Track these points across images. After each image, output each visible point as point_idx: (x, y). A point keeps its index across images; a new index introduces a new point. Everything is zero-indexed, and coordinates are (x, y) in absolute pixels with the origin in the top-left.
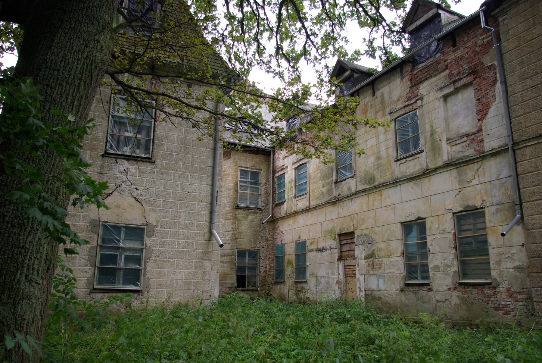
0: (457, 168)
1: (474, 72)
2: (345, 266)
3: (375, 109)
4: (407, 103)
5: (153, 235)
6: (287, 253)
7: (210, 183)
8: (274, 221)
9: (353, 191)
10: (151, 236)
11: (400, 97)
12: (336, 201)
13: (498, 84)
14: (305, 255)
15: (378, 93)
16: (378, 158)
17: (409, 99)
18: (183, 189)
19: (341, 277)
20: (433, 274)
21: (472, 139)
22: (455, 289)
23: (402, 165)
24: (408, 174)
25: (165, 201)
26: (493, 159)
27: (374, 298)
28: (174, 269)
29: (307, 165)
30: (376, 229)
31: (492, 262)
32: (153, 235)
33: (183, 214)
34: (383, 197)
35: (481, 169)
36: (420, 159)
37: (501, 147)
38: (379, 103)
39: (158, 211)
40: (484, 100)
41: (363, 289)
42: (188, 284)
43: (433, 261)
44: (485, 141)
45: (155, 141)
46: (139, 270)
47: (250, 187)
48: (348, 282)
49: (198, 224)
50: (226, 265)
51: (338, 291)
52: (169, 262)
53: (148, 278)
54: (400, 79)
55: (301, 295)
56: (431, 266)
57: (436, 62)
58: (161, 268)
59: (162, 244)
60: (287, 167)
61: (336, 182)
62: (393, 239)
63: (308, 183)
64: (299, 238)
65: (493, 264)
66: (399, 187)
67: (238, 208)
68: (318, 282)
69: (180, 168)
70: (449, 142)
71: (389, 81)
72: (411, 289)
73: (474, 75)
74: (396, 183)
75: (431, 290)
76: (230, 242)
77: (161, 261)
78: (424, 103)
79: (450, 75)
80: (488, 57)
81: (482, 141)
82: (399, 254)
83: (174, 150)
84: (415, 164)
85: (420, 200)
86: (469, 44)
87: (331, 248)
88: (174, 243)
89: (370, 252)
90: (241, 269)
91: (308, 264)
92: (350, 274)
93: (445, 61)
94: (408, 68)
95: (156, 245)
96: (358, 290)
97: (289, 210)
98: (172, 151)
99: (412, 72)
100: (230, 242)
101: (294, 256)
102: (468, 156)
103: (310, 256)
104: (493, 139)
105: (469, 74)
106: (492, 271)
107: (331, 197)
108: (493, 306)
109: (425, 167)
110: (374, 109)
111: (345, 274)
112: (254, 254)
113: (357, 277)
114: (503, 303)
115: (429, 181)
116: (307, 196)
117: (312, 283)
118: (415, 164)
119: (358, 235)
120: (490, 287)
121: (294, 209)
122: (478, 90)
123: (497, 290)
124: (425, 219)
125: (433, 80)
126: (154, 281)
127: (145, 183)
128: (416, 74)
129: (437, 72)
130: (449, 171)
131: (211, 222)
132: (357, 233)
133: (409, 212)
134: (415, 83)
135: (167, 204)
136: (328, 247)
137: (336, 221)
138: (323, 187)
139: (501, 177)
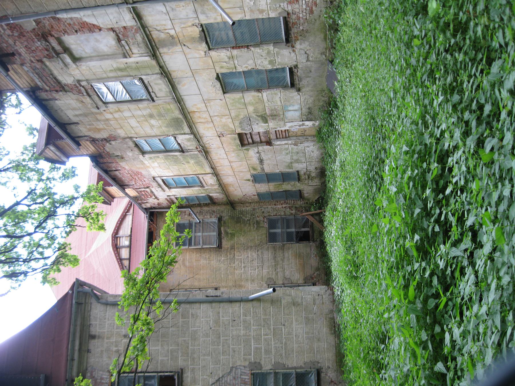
0: (158, 49)
1: (44, 36)
2: (277, 138)
3: (94, 121)
4: (85, 94)
5: (259, 363)
6: (268, 190)
7: (197, 305)
8: (231, 204)
9: (192, 136)
10: (261, 365)
11: (77, 100)
12: (206, 152)
13: (59, 16)
14: (267, 175)
15: (75, 119)
16: (151, 116)
17: (80, 92)
18: (207, 335)
19: (290, 142)
20: (278, 65)
21: (123, 35)
22: (293, 47)
23: (158, 95)
24: (167, 90)
25: (223, 353)
26: (144, 18)
27: (310, 113)
28: (293, 338)
29: (164, 178)
30: (233, 115)
31: (260, 17)
32: (259, 363)
33: (234, 333)
34: (196, 111)
35: (157, 28)
36: (149, 80)
37: (130, 11)
38: (87, 118)
39: (234, 360)
40: (76, 27)
41: (301, 123)
42: (308, 321)
43: (265, 64)
44: (125, 25)
45: (159, 370)
46: (297, 374)
47: (195, 232)
48: (294, 135)
49: (243, 315)
50: (286, 255)
51: (306, 144)
52: (286, 344)
53: (305, 364)
54: (56, 101)
55: (313, 175)
56: (270, 67)
57: (33, 70)
58: (293, 351)
59: (268, 352)
60: (168, 196)
61: (182, 151)
62: (243, 100)
63: (185, 176)
64: (249, 180)
65: (263, 15)
66: (183, 97)
67: (220, 246)
68: (298, 161)
69: (185, 341)
70: (128, 56)
71: (59, 111)
72: (296, 82)
73: (47, 36)
74: (179, 100)
75: (296, 66)
76: (260, 253)
77: (286, 352)
78: (84, 79)
79: (49, 57)
80: (26, 25)
81: (125, 28)
82: (260, 95)
83: (166, 348)
84: (156, 84)
85: (197, 79)
86: (11, 41)
87: (258, 152)
88: (265, 340)
89: (259, 119)
90: (290, 238)
91: (278, 171)
92: (285, 135)
93: (32, 62)
94: (43, 95)
95: (270, 359)
96: (302, 127)
97: (218, 191)
98: (168, 351)
99: (47, 91)
100: (260, 253)
101: (270, 184)
102: (143, 39)
103: (268, 169)
104: (122, 18)
105: (47, 41)
106: (270, 16)
107: (200, 156)
108: (308, 15)
109: (159, 76)
110: (94, 123)
111: (286, 138)
112: (272, 224)
113: (288, 129)
114: (304, 7)
115: (174, 71)
116: (200, 176)
117: (300, 167)
118: (156, 84)
119: (242, 130)
120: (289, 17)
121: (217, 187)
122: (65, 32)
123: (291, 12)
124: (217, 74)
125: (56, 73)
126: (307, 358)
127: (205, 377)
128: (49, 87)
129: (47, 69)
130: (162, 55)
131: (241, 301)
132: (239, 131)
133: (213, 90)
134: (62, 88)
135: (225, 351)
136: (258, 155)
137: (227, 150)
138: (189, 162)
139: (165, 11)
